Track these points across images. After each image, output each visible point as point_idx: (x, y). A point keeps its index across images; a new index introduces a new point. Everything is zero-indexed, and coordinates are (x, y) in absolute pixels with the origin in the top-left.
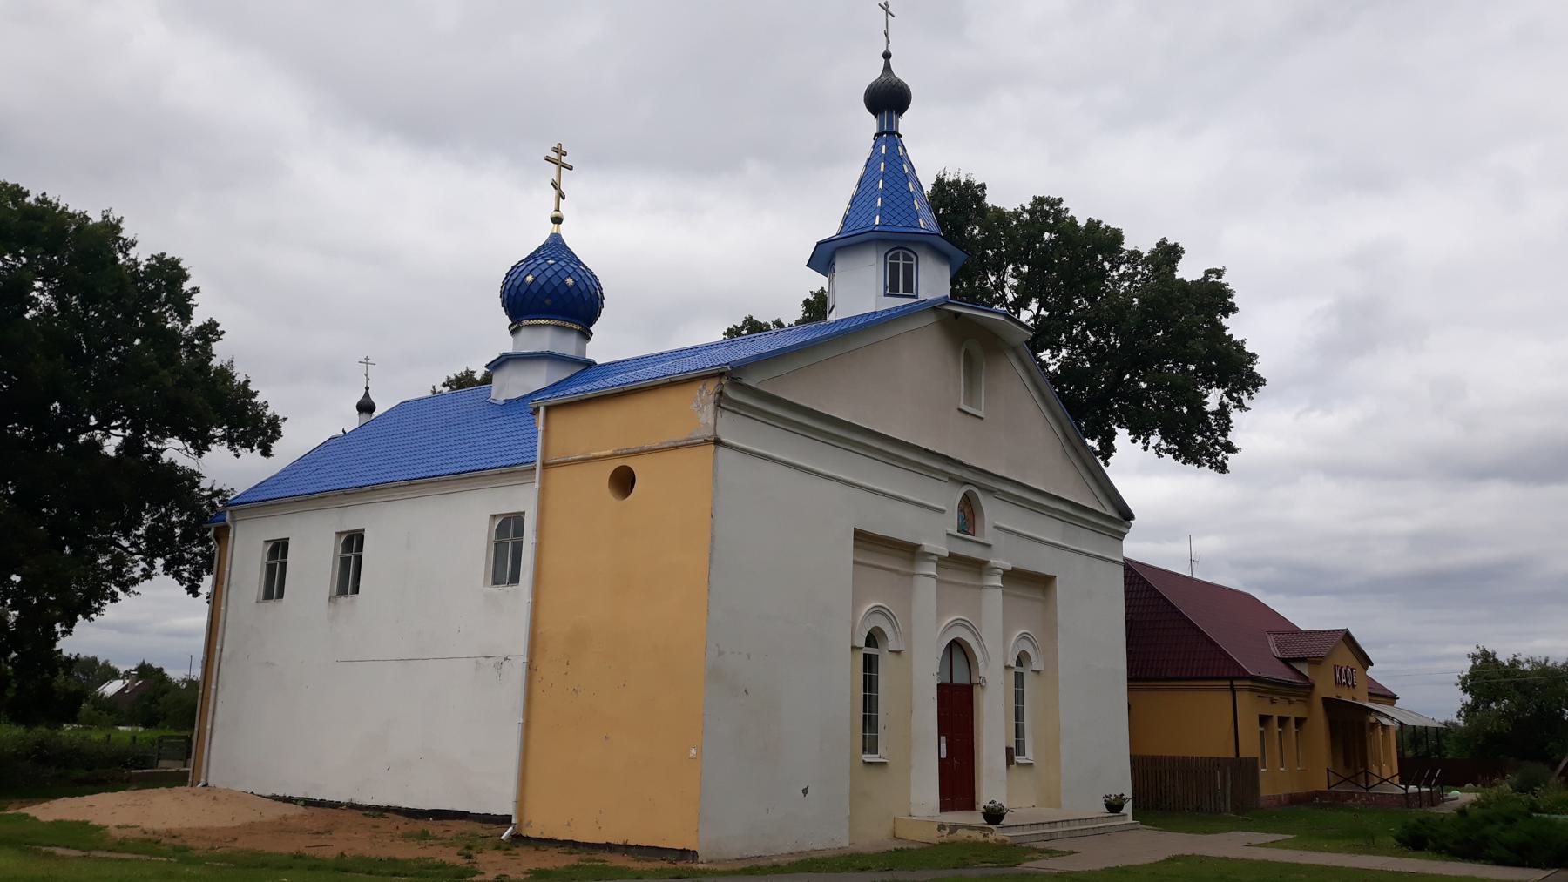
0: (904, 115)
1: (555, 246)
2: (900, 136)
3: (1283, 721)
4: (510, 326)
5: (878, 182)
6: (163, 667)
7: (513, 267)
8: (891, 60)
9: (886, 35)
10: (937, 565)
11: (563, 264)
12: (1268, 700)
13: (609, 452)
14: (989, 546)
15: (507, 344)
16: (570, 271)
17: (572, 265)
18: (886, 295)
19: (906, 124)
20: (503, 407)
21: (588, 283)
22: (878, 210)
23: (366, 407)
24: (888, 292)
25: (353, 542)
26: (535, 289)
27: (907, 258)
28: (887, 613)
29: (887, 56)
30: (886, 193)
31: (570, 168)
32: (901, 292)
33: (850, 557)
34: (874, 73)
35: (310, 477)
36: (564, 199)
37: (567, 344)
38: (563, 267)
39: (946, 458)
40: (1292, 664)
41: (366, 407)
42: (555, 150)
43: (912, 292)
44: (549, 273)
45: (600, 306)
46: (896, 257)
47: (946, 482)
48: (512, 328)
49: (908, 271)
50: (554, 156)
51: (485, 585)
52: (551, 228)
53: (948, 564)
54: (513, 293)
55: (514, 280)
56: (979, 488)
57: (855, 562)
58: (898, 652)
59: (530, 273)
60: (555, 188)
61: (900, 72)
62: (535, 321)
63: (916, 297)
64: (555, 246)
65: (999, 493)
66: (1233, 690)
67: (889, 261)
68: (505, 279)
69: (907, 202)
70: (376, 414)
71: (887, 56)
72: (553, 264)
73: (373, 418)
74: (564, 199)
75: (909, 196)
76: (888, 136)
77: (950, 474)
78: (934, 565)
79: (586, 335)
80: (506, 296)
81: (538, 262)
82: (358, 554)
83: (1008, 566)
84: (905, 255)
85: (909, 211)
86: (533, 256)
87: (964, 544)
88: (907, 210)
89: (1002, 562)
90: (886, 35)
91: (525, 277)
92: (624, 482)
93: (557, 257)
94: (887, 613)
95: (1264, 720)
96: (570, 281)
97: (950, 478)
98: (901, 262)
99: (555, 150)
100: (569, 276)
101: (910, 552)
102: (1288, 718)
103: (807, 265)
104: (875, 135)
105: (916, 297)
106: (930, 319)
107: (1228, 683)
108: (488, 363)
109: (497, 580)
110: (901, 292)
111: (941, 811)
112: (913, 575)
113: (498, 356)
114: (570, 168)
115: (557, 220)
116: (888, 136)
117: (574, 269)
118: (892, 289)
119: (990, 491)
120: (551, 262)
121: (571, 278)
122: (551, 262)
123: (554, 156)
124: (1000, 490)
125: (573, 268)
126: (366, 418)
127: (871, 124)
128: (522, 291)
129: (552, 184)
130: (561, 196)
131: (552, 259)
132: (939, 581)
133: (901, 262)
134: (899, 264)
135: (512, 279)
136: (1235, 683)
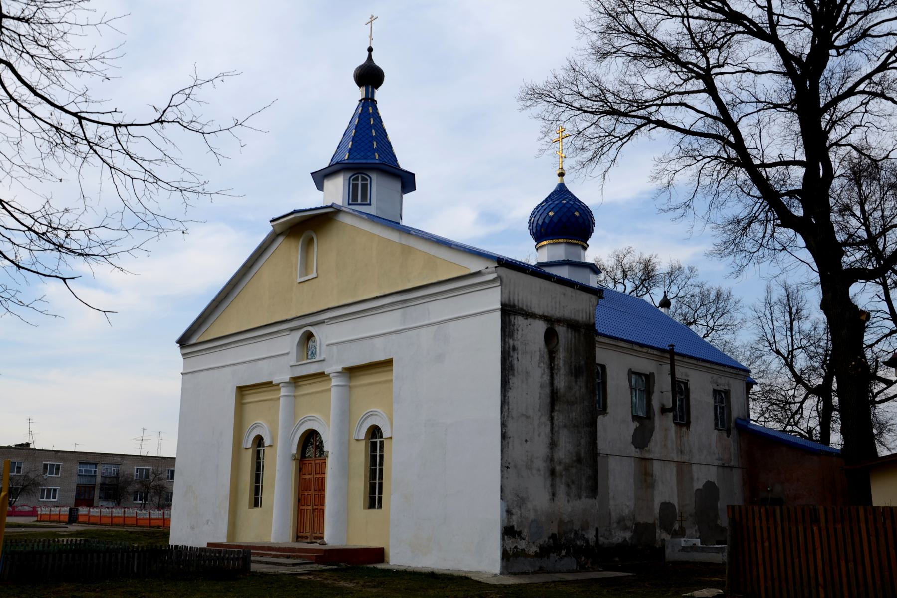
0: (379, 88)
1: (561, 191)
4: (536, 246)
5: (372, 131)
16: (577, 207)
19: (379, 94)
24: (350, 202)
26: (555, 220)
27: (364, 179)
29: (370, 50)
32: (359, 202)
34: (362, 60)
38: (572, 205)
39: (329, 309)
44: (565, 210)
45: (591, 225)
46: (356, 179)
48: (537, 247)
49: (364, 187)
52: (558, 180)
61: (378, 61)
64: (561, 191)
67: (351, 182)
71: (370, 50)
72: (565, 204)
76: (368, 103)
81: (549, 204)
83: (339, 368)
84: (362, 177)
87: (303, 367)
89: (333, 367)
93: (567, 198)
96: (577, 214)
98: (360, 183)
100: (577, 210)
103: (312, 174)
110: (359, 202)
116: (368, 103)
127: (359, 93)
133: (360, 183)
134: (367, 184)
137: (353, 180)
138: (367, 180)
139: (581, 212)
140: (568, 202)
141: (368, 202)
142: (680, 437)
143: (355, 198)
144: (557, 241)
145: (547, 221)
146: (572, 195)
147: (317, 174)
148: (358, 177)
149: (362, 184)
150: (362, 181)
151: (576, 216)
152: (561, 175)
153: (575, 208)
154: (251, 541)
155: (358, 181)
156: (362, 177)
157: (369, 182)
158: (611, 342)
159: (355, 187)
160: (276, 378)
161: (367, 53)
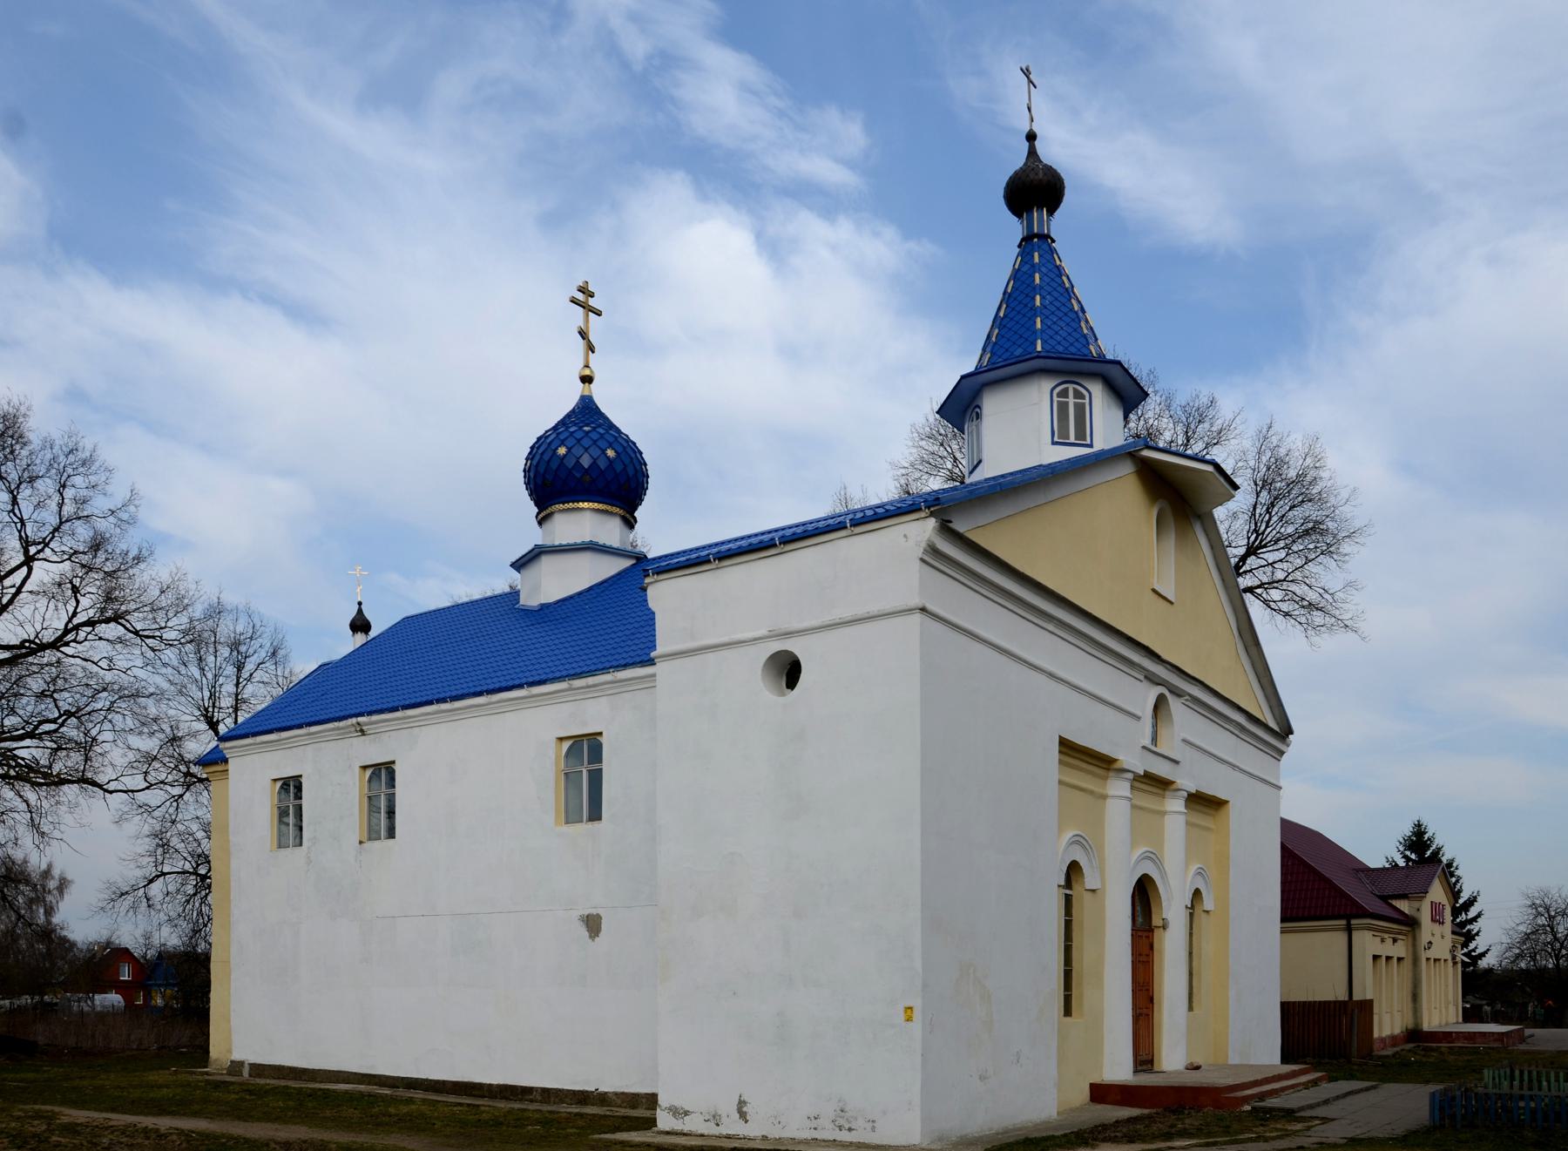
1: (587, 411)
2: (1053, 241)
3: (1388, 958)
6: (601, 912)
7: (539, 439)
8: (1036, 142)
9: (1029, 109)
10: (1132, 787)
11: (602, 431)
12: (1379, 939)
13: (763, 632)
14: (1177, 762)
15: (535, 536)
16: (611, 440)
17: (611, 432)
18: (1054, 443)
19: (1060, 225)
20: (541, 612)
21: (633, 456)
22: (1039, 334)
23: (360, 624)
25: (383, 773)
26: (570, 463)
27: (1078, 395)
28: (1084, 842)
30: (1047, 312)
31: (599, 313)
33: (1056, 777)
34: (1018, 160)
35: (280, 715)
36: (593, 352)
37: (608, 530)
40: (1390, 901)
41: (360, 624)
42: (582, 290)
43: (1085, 440)
46: (1064, 394)
47: (1141, 681)
48: (540, 517)
49: (1080, 410)
50: (580, 296)
51: (557, 823)
52: (578, 389)
53: (1145, 781)
54: (542, 470)
55: (542, 454)
56: (1170, 691)
57: (1061, 782)
58: (1093, 891)
59: (562, 443)
60: (584, 339)
61: (1050, 153)
62: (571, 505)
63: (1091, 446)
64: (587, 411)
65: (1187, 697)
66: (1349, 930)
67: (1055, 399)
68: (530, 453)
69: (1073, 324)
70: (373, 633)
72: (589, 432)
73: (369, 638)
74: (593, 352)
75: (1073, 316)
76: (1035, 243)
77: (1147, 670)
78: (1127, 785)
79: (630, 523)
80: (532, 475)
82: (390, 791)
84: (1076, 391)
85: (1076, 335)
86: (562, 423)
88: (1074, 334)
90: (1029, 109)
91: (557, 449)
92: (789, 671)
93: (593, 423)
94: (1084, 842)
95: (1376, 957)
96: (611, 453)
97: (1146, 677)
99: (582, 290)
100: (611, 446)
101: (1104, 763)
102: (1380, 956)
104: (1022, 240)
105: (1091, 446)
106: (1126, 469)
107: (1344, 922)
108: (514, 560)
109: (571, 817)
110: (1072, 439)
111: (1091, 1084)
112: (1164, 813)
113: (530, 548)
114: (599, 313)
115: (586, 380)
116: (1035, 243)
117: (616, 438)
118: (1059, 439)
119: (1178, 693)
120: (586, 429)
121: (613, 449)
122: (586, 429)
123: (580, 296)
124: (1190, 695)
125: (614, 436)
126: (360, 639)
127: (1014, 228)
128: (554, 465)
129: (580, 333)
130: (591, 348)
131: (587, 425)
132: (1134, 807)
133: (1071, 400)
134: (1084, 404)
135: (540, 451)
136: (1353, 922)
137: (1059, 395)
138: (1083, 397)
139: (620, 449)
140: (594, 429)
141: (1088, 442)
142: (1153, 857)
143: (1064, 432)
144: (609, 508)
145: (602, 464)
146: (607, 419)
147: (958, 388)
148: (1067, 389)
149: (1075, 404)
150: (1075, 397)
151: (608, 458)
152: (586, 380)
153: (608, 442)
154: (1123, 1079)
155: (1068, 397)
156: (1075, 389)
157: (1087, 401)
158: (587, 690)
159: (1063, 408)
160: (1183, 782)
161: (1027, 144)
